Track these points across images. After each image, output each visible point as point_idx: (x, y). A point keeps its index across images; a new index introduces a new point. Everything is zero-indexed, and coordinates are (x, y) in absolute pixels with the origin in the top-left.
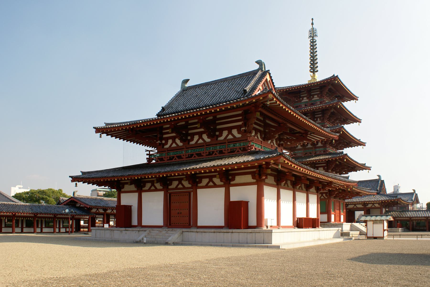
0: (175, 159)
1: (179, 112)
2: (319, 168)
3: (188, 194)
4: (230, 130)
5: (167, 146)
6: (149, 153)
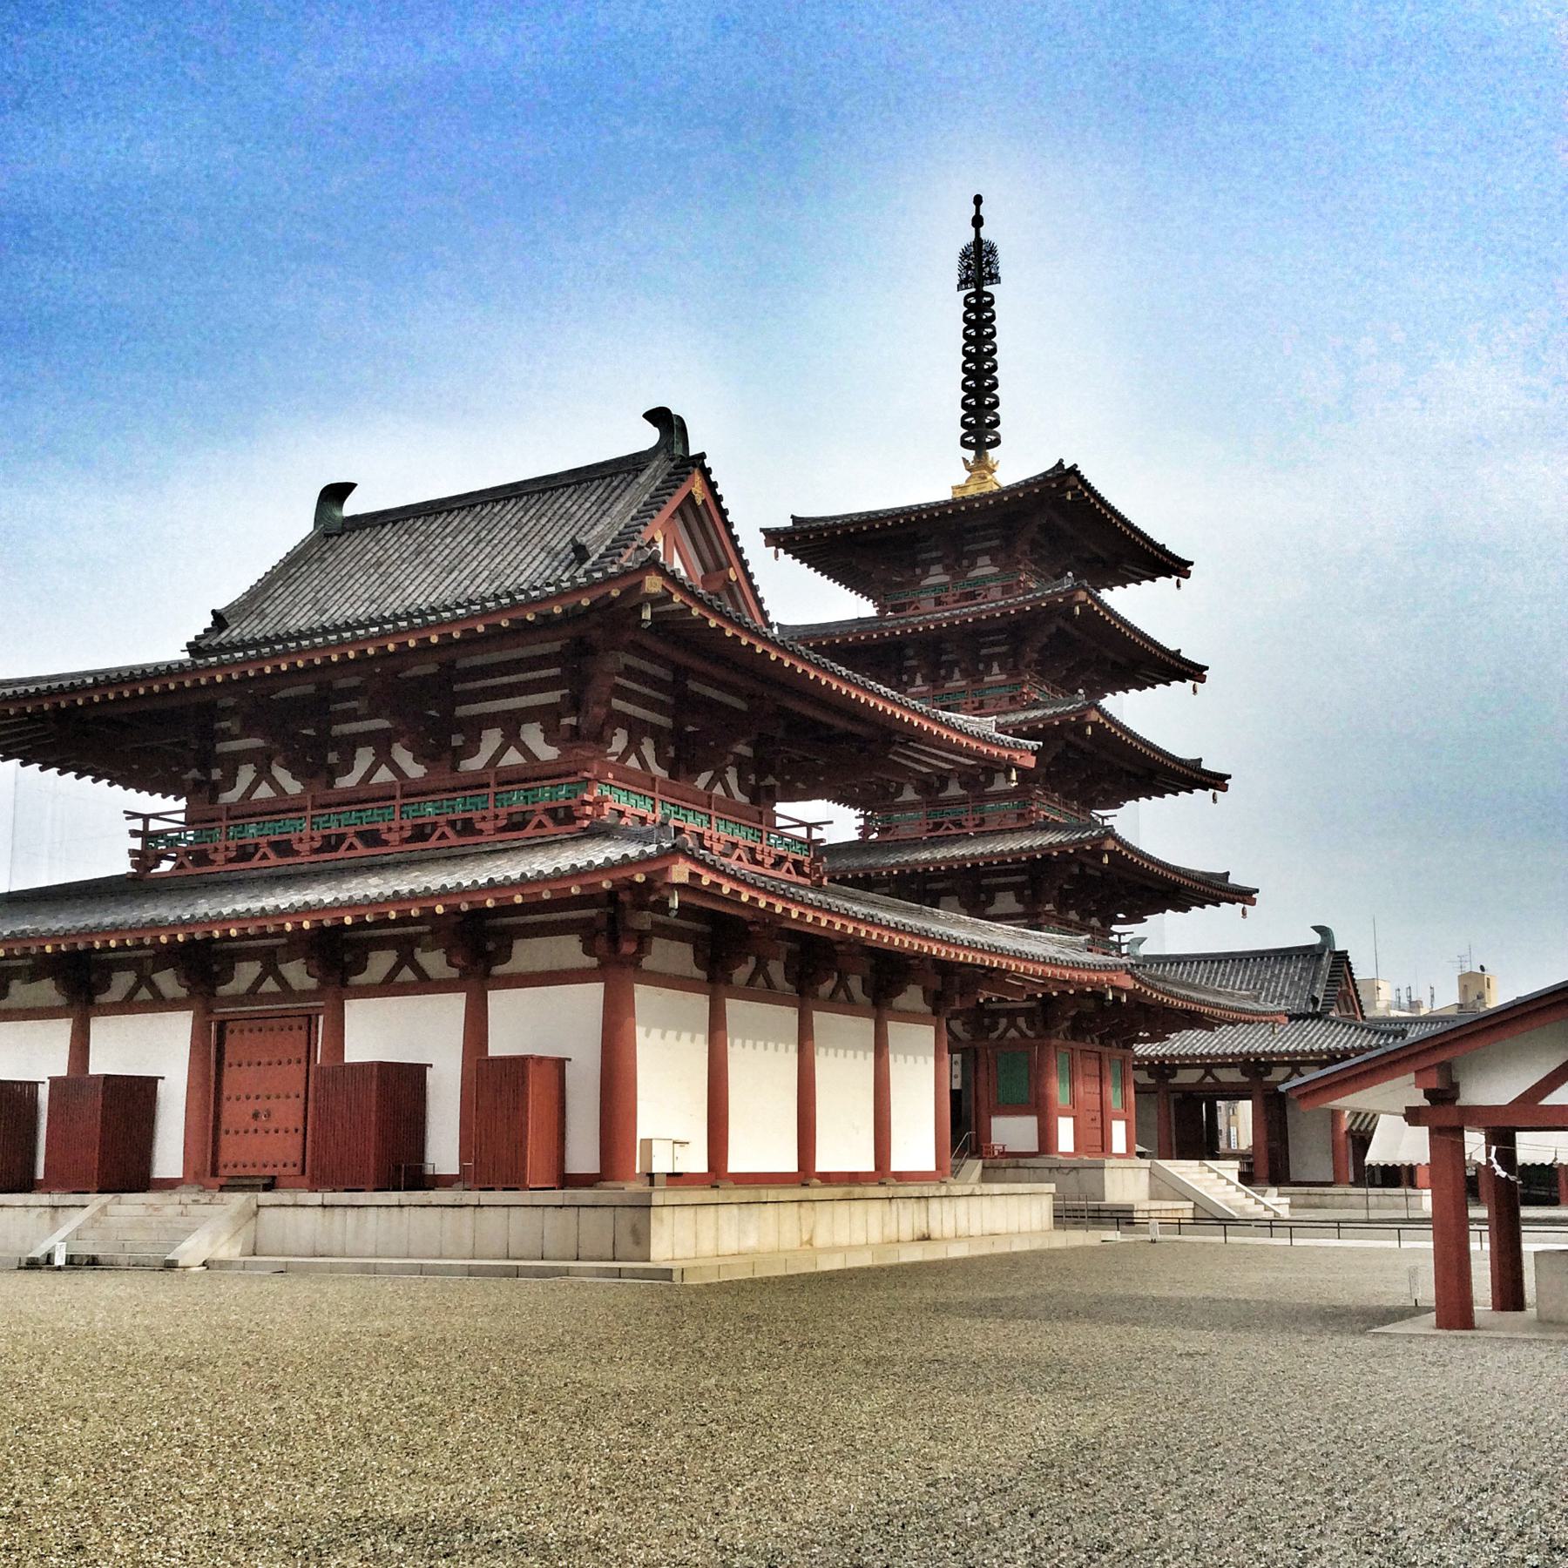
0: (265, 857)
1: (291, 638)
2: (944, 899)
3: (303, 1022)
4: (511, 726)
5: (230, 797)
6: (146, 825)
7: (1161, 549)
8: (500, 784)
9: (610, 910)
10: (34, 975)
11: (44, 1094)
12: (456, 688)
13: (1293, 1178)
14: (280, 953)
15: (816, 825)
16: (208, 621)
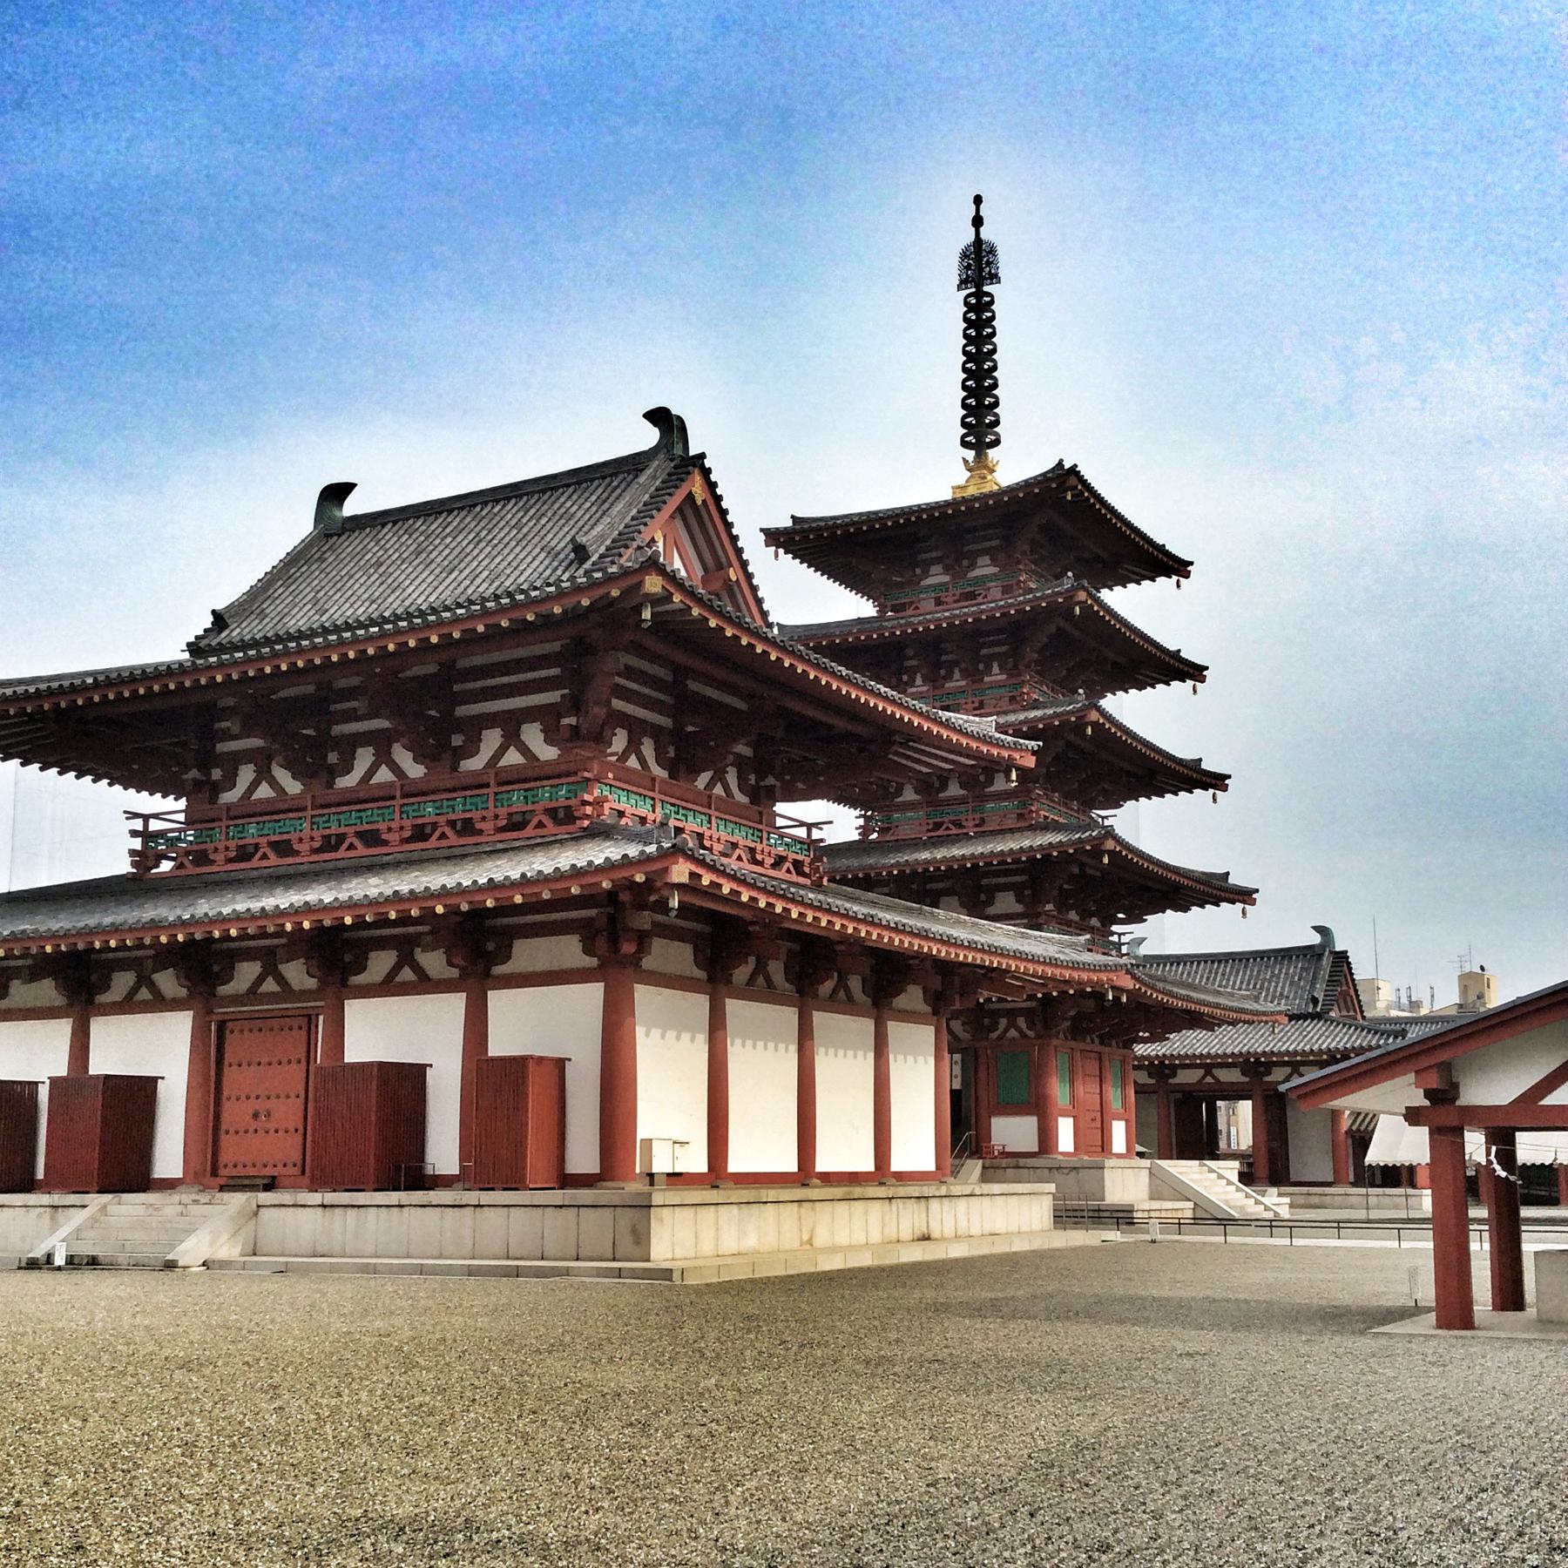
0: (265, 857)
1: (291, 638)
2: (944, 899)
3: (303, 1022)
4: (511, 726)
5: (230, 797)
6: (146, 825)
7: (1161, 549)
8: (500, 784)
9: (610, 910)
10: (34, 975)
11: (44, 1094)
12: (456, 688)
13: (1293, 1178)
14: (280, 953)
15: (816, 825)
16: (208, 621)
